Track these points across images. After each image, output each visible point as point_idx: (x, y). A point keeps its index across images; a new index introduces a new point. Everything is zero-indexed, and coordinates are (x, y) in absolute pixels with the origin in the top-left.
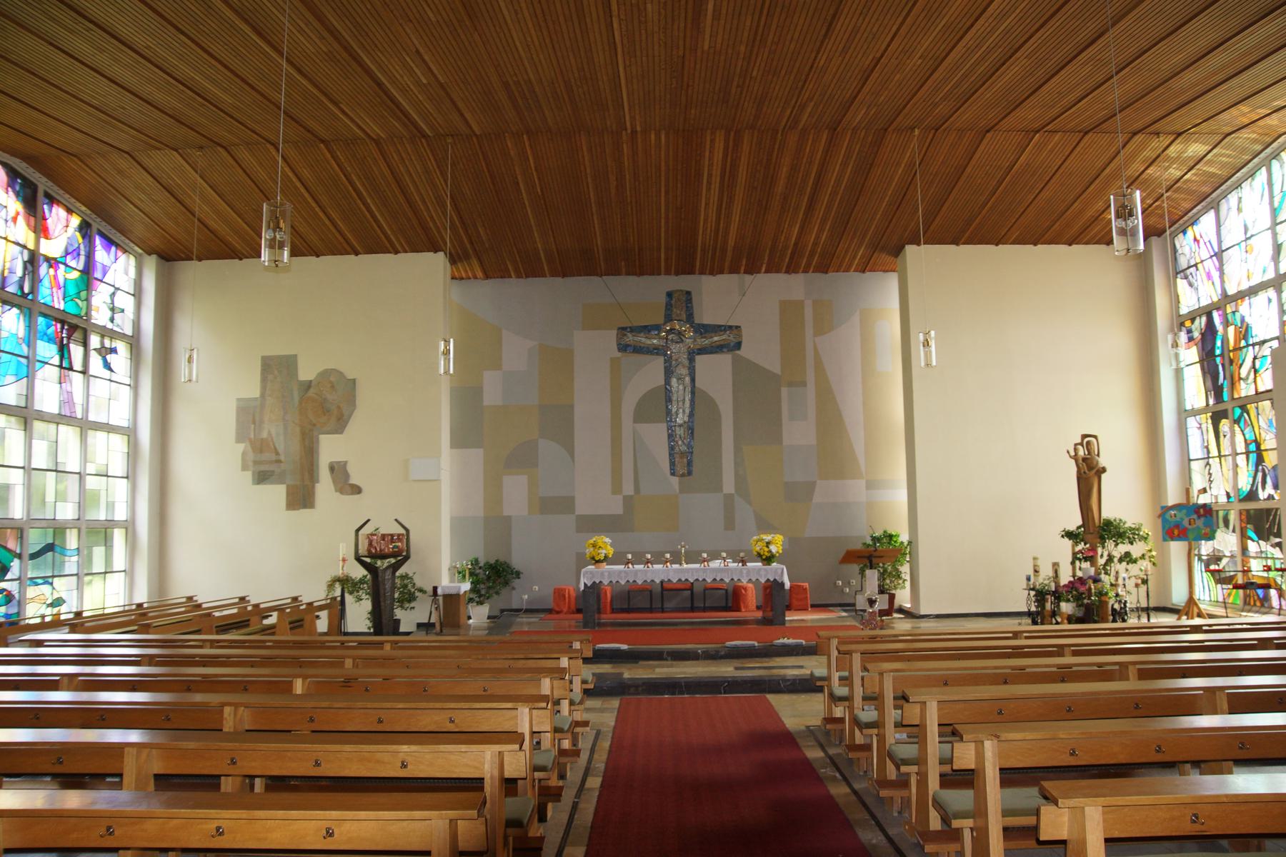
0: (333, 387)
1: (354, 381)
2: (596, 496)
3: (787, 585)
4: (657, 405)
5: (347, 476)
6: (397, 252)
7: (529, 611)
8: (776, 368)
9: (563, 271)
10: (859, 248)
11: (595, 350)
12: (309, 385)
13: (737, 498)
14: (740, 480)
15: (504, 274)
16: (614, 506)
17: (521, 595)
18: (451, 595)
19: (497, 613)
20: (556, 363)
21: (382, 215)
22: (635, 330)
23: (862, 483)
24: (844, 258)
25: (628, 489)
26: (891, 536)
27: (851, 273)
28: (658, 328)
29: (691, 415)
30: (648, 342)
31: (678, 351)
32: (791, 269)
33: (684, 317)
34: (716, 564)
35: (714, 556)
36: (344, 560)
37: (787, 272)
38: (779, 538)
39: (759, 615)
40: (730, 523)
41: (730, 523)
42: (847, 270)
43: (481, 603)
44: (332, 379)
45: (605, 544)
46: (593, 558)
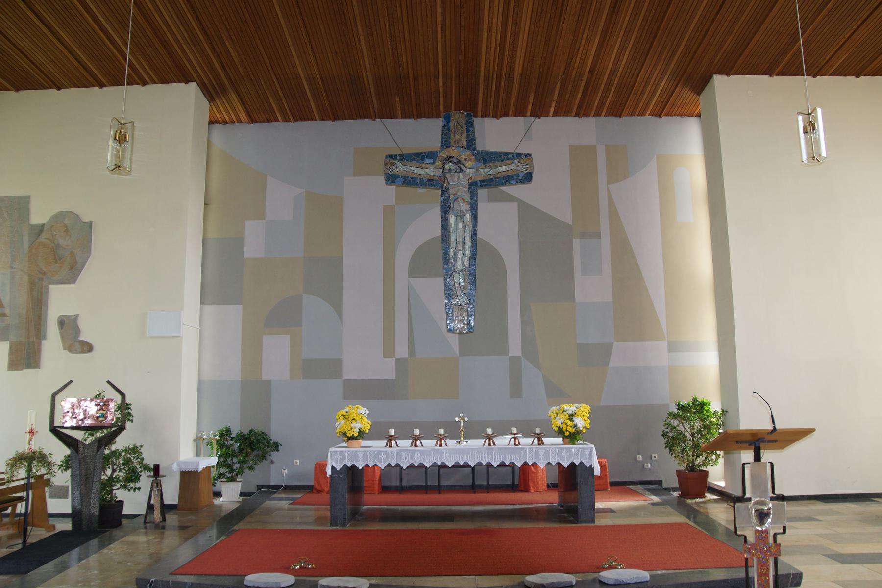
0: (67, 231)
1: (91, 223)
2: (366, 360)
3: (597, 471)
4: (436, 258)
5: (77, 331)
6: (144, 83)
7: (288, 488)
8: (567, 217)
9: (334, 114)
10: (662, 77)
11: (368, 197)
12: (40, 229)
13: (524, 361)
14: (528, 341)
15: (270, 118)
16: (386, 370)
17: (282, 469)
18: (189, 473)
19: (253, 489)
20: (324, 213)
21: (107, 19)
22: (403, 158)
23: (663, 345)
24: (642, 93)
25: (402, 351)
26: (702, 405)
27: (647, 118)
28: (432, 155)
29: (473, 257)
30: (421, 172)
31: (459, 184)
32: (582, 111)
33: (464, 142)
34: (503, 441)
35: (502, 429)
36: (32, 432)
37: (577, 115)
38: (585, 409)
39: (553, 499)
40: (516, 390)
41: (516, 390)
42: (642, 114)
43: (232, 479)
44: (66, 222)
45: (360, 416)
46: (345, 434)
